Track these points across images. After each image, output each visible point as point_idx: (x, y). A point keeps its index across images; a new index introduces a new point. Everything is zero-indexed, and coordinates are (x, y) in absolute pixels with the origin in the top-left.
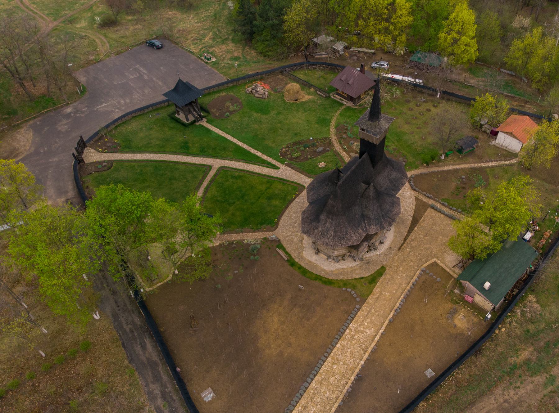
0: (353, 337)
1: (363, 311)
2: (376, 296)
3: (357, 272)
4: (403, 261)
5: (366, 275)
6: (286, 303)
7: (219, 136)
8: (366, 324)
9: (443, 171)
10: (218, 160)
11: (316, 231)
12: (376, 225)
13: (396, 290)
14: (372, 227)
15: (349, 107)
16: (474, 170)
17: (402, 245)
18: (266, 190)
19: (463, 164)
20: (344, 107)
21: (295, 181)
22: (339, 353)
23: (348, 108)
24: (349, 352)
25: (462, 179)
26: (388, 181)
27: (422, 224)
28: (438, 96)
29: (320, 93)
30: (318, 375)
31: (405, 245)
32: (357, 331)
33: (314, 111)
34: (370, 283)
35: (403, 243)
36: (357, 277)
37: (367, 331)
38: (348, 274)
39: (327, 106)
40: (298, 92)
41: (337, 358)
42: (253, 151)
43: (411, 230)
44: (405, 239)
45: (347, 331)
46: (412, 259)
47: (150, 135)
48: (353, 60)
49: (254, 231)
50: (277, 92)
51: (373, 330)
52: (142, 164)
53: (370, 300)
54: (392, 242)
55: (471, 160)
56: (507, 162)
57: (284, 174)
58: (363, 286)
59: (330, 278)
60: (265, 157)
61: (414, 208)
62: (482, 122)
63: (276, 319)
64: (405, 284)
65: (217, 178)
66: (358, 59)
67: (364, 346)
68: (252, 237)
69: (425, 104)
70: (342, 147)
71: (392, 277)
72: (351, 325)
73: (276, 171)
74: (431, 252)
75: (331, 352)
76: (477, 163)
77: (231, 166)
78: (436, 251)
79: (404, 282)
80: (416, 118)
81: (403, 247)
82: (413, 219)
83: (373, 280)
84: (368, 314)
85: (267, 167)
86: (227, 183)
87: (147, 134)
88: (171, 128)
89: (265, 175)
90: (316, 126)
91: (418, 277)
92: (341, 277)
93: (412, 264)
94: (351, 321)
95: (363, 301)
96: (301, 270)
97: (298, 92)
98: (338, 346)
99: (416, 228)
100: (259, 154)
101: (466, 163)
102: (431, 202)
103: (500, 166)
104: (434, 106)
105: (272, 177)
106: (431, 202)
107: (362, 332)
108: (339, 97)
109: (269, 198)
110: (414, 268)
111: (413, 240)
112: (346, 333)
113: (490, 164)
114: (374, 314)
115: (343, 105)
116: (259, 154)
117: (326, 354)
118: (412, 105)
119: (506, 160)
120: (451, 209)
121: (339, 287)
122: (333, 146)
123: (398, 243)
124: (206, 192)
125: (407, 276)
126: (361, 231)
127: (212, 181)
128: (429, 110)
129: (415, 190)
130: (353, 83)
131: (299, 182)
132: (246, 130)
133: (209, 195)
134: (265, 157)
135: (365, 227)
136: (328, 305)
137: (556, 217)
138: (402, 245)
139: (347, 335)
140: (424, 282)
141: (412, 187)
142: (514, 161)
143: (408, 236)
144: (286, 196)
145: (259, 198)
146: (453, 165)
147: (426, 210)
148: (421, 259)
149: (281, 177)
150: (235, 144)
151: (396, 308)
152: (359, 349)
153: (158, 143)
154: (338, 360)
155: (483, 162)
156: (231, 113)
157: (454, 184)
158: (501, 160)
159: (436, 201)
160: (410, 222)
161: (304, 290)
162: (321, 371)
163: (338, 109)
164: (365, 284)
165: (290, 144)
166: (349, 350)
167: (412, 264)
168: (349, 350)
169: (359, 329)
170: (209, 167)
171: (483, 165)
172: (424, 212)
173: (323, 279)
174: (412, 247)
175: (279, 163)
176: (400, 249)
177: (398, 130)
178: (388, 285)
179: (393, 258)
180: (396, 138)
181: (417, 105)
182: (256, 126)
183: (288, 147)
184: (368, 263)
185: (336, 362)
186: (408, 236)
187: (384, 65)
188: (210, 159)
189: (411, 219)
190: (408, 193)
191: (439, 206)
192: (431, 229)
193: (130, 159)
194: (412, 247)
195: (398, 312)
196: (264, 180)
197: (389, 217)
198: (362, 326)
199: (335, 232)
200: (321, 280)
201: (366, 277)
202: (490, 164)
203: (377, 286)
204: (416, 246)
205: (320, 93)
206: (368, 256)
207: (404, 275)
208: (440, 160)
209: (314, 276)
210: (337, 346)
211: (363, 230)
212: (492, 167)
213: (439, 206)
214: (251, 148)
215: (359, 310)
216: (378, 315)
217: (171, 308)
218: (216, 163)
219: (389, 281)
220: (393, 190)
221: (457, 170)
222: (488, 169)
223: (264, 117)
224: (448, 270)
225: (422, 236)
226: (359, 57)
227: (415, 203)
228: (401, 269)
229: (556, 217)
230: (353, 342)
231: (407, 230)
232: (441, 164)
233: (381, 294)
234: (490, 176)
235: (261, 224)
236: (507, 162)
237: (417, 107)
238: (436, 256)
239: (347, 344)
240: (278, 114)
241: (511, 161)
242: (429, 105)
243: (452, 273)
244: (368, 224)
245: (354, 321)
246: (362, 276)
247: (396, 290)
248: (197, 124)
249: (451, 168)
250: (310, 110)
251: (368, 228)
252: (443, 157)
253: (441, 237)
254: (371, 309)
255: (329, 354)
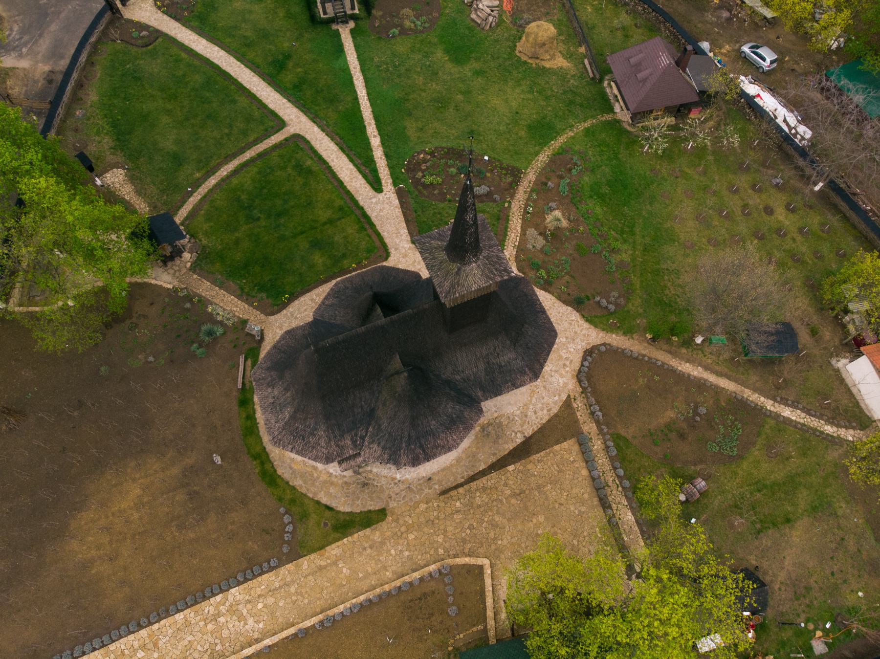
0: (215, 617)
1: (277, 576)
2: (323, 563)
3: (332, 490)
4: (430, 522)
5: (342, 509)
6: (175, 471)
7: (346, 71)
8: (260, 606)
9: (673, 371)
10: (304, 119)
11: (270, 390)
12: (384, 448)
13: (367, 575)
14: (375, 446)
15: (619, 122)
16: (740, 406)
17: (456, 487)
18: (325, 224)
19: (729, 378)
20: (609, 117)
21: (385, 234)
22: (170, 631)
23: (616, 124)
24: (186, 642)
25: (696, 413)
26: (482, 366)
27: (529, 467)
28: (817, 188)
29: (588, 66)
30: (102, 651)
31: (461, 490)
32: (233, 610)
33: (547, 98)
34: (336, 528)
35: (461, 485)
36: (325, 501)
37: (251, 622)
38: (313, 484)
39: (578, 100)
40: (544, 44)
41: (158, 640)
42: (372, 130)
43: (500, 464)
44: (472, 479)
45: (219, 598)
46: (449, 529)
47: (250, 12)
48: (718, 17)
49: (239, 297)
50: (515, 24)
51: (261, 625)
52: (197, 63)
53: (305, 563)
54: (443, 470)
55: (754, 378)
56: (829, 429)
57: (379, 207)
58: (318, 525)
59: (280, 472)
60: (378, 154)
61: (544, 421)
62: (851, 306)
63: (135, 491)
64: (394, 572)
65: (274, 154)
66: (729, 20)
67: (218, 647)
68: (227, 305)
69: (773, 191)
70: (526, 205)
71: (382, 543)
72: (233, 591)
73: (372, 193)
74: (495, 539)
75: (158, 621)
76: (762, 393)
77: (313, 143)
78: (505, 542)
79: (394, 568)
80: (727, 217)
81: (453, 493)
82: (523, 443)
83: (346, 525)
84: (280, 587)
85: (365, 177)
86: (279, 173)
87: (248, 6)
88: (289, 16)
89: (348, 193)
90: (523, 133)
91: (422, 579)
92: (297, 483)
93: (440, 539)
94: (239, 584)
95: (294, 555)
96: (249, 423)
97: (544, 44)
98: (179, 617)
99: (511, 468)
100: (375, 141)
101: (736, 380)
102: (589, 428)
103: (803, 429)
104: (787, 207)
105: (356, 203)
106: (589, 428)
107: (241, 618)
108: (616, 91)
109: (316, 245)
110: (436, 550)
111: (484, 489)
112: (212, 600)
113: (787, 412)
114: (290, 595)
115: (611, 110)
116: (375, 141)
117: (144, 621)
118: (743, 181)
119: (832, 424)
120: (615, 469)
121: (280, 499)
122: (512, 196)
123: (452, 479)
124: (235, 172)
125: (410, 558)
126: (349, 442)
127: (261, 156)
128: (769, 211)
129: (580, 381)
130: (644, 81)
131: (387, 241)
132: (397, 80)
133: (235, 181)
134: (378, 154)
135: (363, 438)
136: (233, 523)
137: (819, 633)
138: (456, 487)
139: (209, 607)
140: (425, 595)
141: (579, 371)
142: (849, 435)
143: (483, 473)
144: (344, 256)
145: (302, 233)
146: (706, 368)
147: (565, 440)
148: (464, 541)
149: (369, 212)
150: (356, 99)
151: (330, 613)
152: (206, 647)
153: (248, 34)
154: (155, 645)
155: (775, 400)
156: (403, 32)
157: (671, 414)
158: (820, 417)
159: (600, 430)
160: (511, 446)
161: (221, 466)
162: (112, 647)
163: (593, 117)
164: (326, 524)
165: (443, 148)
166: (190, 638)
167: (440, 539)
168: (190, 638)
169: (240, 607)
170: (281, 124)
171: (769, 405)
172: (557, 442)
173: (267, 466)
174: (470, 505)
175: (390, 181)
176: (444, 492)
177: (668, 225)
178: (360, 554)
179: (417, 505)
180: (648, 240)
181: (753, 187)
182: (420, 80)
183: (432, 154)
184: (365, 485)
185: (150, 646)
186: (483, 473)
187: (764, 59)
188: (295, 110)
189: (519, 441)
190: (561, 381)
191: (597, 445)
192: (539, 487)
193: (186, 43)
194: (470, 505)
195: (331, 625)
196: (339, 202)
197: (421, 446)
198: (249, 606)
199: (293, 417)
200: (262, 463)
201: (339, 512)
202: (787, 412)
203: (340, 543)
204: (479, 506)
205: (588, 66)
206: (375, 470)
207: (407, 553)
208: (688, 343)
209: (258, 449)
210: (177, 616)
211: (354, 442)
212: (787, 421)
213: (597, 445)
214: (373, 122)
215: (271, 569)
216: (294, 602)
217: (13, 363)
218: (297, 122)
219: (371, 547)
220: (483, 389)
221: (701, 386)
222: (772, 422)
223: (449, 66)
224: (489, 602)
225: (508, 492)
226: (736, 16)
227: (555, 410)
228: (411, 537)
229: (819, 633)
230: (210, 627)
231: (492, 459)
232: (684, 351)
233: (335, 563)
234: (760, 441)
235: (262, 288)
236: (829, 429)
237: (750, 191)
238: (494, 556)
239: (197, 623)
240: (478, 73)
241: (842, 432)
242: (778, 202)
243: (490, 613)
244: (371, 437)
245: (246, 585)
246: (334, 505)
247: (367, 575)
248: (334, 27)
249: (695, 371)
250: (540, 93)
251: (366, 443)
252: (699, 340)
253: (541, 518)
254: (293, 581)
255: (151, 624)
